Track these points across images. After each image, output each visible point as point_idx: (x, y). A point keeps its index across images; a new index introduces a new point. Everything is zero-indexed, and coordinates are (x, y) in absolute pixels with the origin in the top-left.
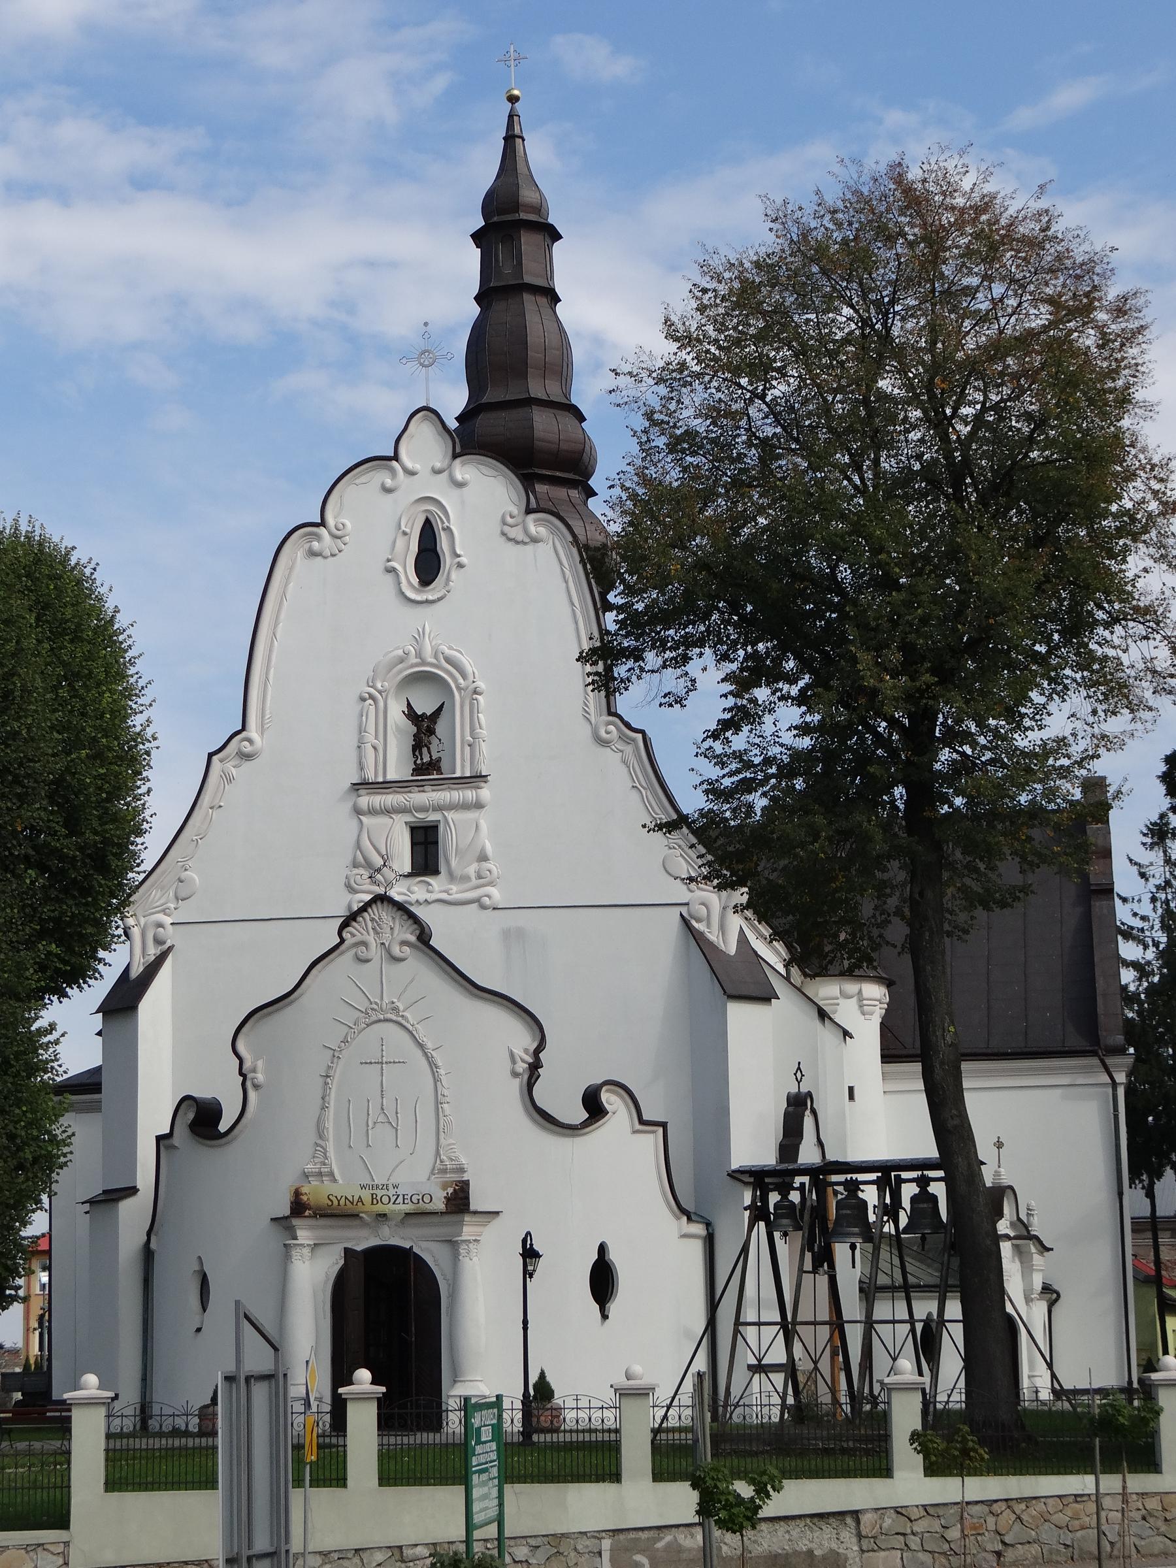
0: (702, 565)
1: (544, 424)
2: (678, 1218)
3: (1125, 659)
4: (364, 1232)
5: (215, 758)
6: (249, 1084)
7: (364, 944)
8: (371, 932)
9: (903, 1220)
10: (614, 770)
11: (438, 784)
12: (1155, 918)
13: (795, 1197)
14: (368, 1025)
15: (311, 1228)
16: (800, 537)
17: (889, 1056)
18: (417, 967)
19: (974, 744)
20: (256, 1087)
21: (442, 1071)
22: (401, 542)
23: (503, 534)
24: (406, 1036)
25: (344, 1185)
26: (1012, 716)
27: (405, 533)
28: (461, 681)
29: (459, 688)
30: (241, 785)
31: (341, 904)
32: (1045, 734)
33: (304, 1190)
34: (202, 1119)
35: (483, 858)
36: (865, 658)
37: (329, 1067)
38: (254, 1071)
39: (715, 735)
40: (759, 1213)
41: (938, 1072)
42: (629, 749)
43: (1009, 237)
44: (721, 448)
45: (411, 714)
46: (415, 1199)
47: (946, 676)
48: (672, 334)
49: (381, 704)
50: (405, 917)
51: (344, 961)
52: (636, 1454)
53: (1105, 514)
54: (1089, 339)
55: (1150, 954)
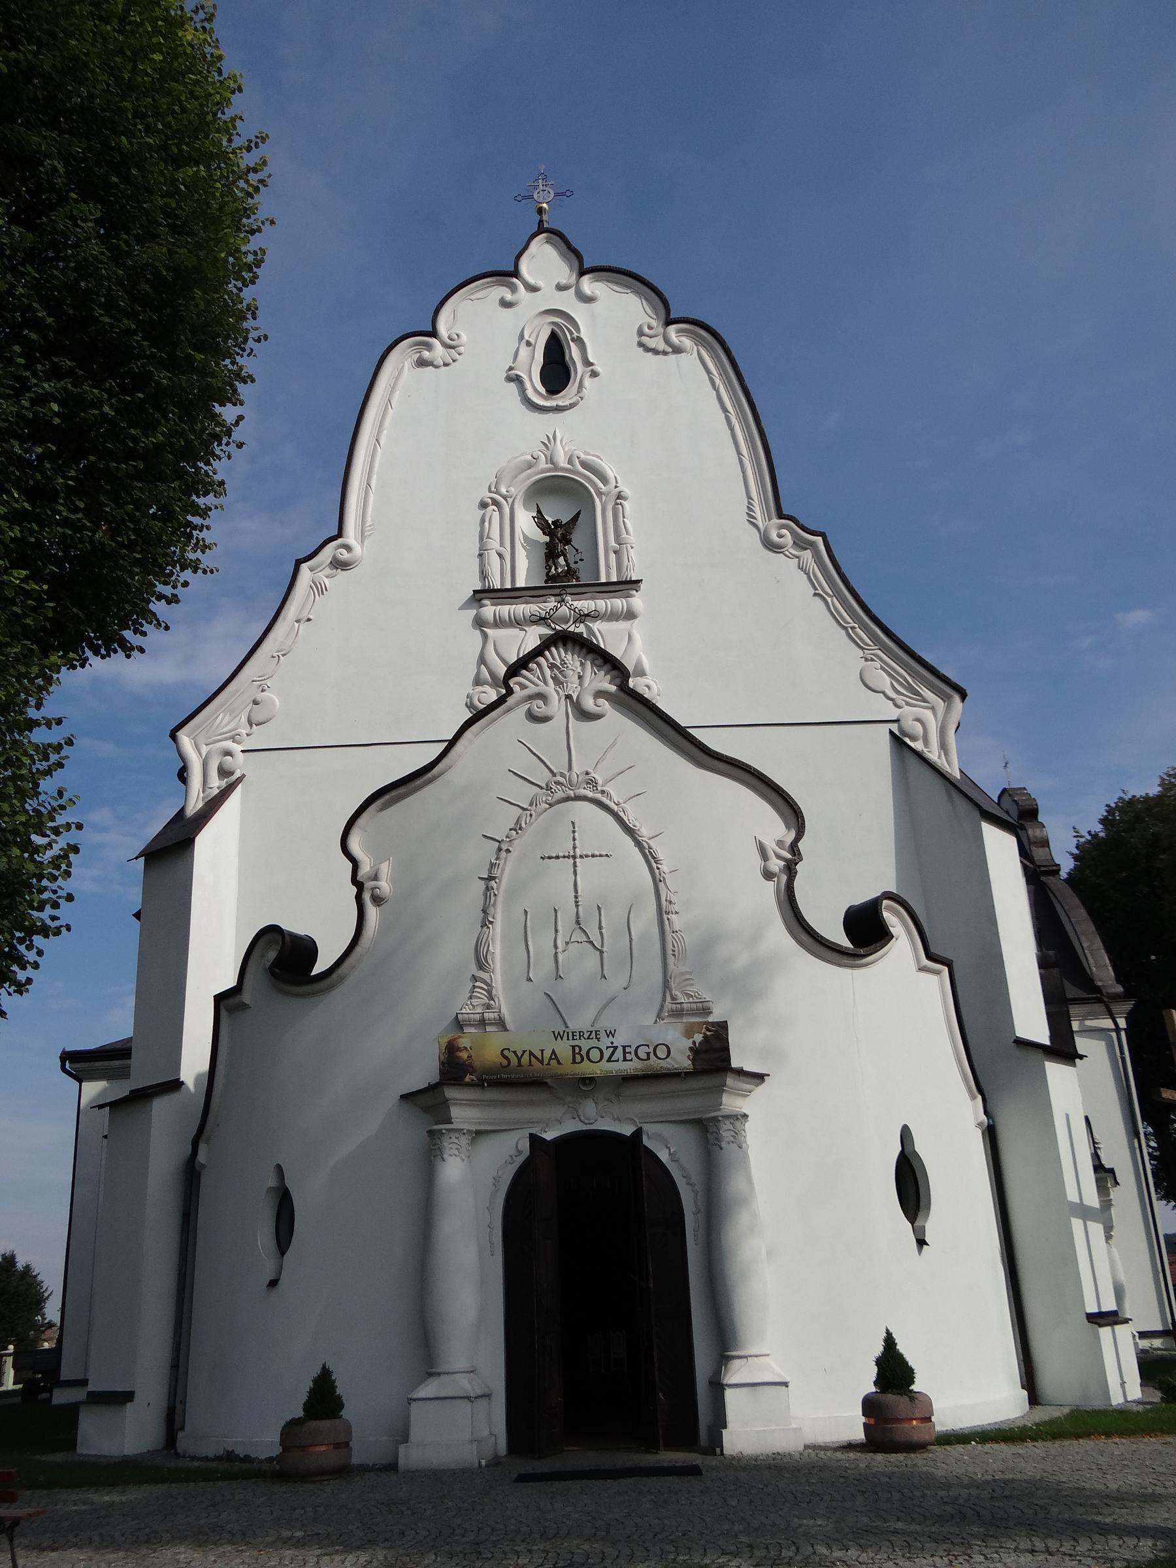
2: (973, 1098)
4: (557, 1111)
5: (304, 567)
6: (367, 897)
7: (542, 696)
8: (551, 681)
14: (551, 805)
15: (471, 1103)
18: (616, 721)
20: (378, 900)
21: (664, 868)
22: (524, 352)
23: (641, 344)
24: (609, 819)
25: (518, 1019)
27: (528, 344)
28: (600, 485)
29: (600, 494)
33: (464, 1042)
34: (281, 959)
37: (492, 865)
38: (376, 878)
42: (807, 555)
46: (642, 1053)
49: (507, 510)
50: (599, 662)
51: (511, 721)
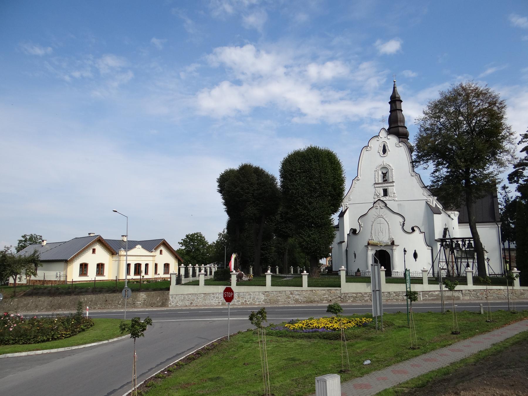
0: (430, 147)
1: (401, 129)
3: (503, 159)
9: (466, 247)
10: (414, 181)
11: (387, 183)
12: (504, 201)
13: (448, 243)
16: (446, 143)
17: (460, 222)
18: (385, 210)
19: (477, 173)
25: (375, 241)
26: (484, 169)
30: (357, 184)
31: (373, 201)
32: (489, 171)
34: (354, 232)
35: (394, 193)
36: (458, 161)
39: (433, 173)
40: (442, 245)
41: (472, 224)
43: (481, 93)
44: (433, 130)
45: (382, 173)
47: (472, 163)
48: (424, 113)
51: (374, 209)
52: (425, 280)
53: (499, 136)
54: (495, 108)
55: (503, 207)
